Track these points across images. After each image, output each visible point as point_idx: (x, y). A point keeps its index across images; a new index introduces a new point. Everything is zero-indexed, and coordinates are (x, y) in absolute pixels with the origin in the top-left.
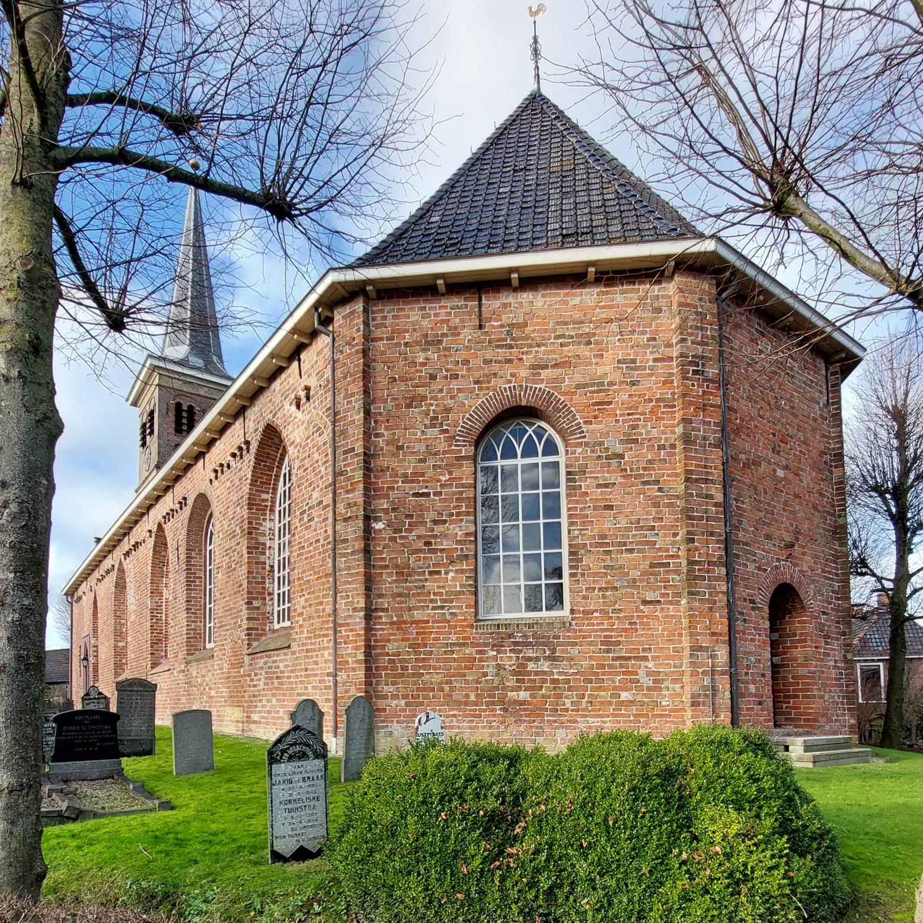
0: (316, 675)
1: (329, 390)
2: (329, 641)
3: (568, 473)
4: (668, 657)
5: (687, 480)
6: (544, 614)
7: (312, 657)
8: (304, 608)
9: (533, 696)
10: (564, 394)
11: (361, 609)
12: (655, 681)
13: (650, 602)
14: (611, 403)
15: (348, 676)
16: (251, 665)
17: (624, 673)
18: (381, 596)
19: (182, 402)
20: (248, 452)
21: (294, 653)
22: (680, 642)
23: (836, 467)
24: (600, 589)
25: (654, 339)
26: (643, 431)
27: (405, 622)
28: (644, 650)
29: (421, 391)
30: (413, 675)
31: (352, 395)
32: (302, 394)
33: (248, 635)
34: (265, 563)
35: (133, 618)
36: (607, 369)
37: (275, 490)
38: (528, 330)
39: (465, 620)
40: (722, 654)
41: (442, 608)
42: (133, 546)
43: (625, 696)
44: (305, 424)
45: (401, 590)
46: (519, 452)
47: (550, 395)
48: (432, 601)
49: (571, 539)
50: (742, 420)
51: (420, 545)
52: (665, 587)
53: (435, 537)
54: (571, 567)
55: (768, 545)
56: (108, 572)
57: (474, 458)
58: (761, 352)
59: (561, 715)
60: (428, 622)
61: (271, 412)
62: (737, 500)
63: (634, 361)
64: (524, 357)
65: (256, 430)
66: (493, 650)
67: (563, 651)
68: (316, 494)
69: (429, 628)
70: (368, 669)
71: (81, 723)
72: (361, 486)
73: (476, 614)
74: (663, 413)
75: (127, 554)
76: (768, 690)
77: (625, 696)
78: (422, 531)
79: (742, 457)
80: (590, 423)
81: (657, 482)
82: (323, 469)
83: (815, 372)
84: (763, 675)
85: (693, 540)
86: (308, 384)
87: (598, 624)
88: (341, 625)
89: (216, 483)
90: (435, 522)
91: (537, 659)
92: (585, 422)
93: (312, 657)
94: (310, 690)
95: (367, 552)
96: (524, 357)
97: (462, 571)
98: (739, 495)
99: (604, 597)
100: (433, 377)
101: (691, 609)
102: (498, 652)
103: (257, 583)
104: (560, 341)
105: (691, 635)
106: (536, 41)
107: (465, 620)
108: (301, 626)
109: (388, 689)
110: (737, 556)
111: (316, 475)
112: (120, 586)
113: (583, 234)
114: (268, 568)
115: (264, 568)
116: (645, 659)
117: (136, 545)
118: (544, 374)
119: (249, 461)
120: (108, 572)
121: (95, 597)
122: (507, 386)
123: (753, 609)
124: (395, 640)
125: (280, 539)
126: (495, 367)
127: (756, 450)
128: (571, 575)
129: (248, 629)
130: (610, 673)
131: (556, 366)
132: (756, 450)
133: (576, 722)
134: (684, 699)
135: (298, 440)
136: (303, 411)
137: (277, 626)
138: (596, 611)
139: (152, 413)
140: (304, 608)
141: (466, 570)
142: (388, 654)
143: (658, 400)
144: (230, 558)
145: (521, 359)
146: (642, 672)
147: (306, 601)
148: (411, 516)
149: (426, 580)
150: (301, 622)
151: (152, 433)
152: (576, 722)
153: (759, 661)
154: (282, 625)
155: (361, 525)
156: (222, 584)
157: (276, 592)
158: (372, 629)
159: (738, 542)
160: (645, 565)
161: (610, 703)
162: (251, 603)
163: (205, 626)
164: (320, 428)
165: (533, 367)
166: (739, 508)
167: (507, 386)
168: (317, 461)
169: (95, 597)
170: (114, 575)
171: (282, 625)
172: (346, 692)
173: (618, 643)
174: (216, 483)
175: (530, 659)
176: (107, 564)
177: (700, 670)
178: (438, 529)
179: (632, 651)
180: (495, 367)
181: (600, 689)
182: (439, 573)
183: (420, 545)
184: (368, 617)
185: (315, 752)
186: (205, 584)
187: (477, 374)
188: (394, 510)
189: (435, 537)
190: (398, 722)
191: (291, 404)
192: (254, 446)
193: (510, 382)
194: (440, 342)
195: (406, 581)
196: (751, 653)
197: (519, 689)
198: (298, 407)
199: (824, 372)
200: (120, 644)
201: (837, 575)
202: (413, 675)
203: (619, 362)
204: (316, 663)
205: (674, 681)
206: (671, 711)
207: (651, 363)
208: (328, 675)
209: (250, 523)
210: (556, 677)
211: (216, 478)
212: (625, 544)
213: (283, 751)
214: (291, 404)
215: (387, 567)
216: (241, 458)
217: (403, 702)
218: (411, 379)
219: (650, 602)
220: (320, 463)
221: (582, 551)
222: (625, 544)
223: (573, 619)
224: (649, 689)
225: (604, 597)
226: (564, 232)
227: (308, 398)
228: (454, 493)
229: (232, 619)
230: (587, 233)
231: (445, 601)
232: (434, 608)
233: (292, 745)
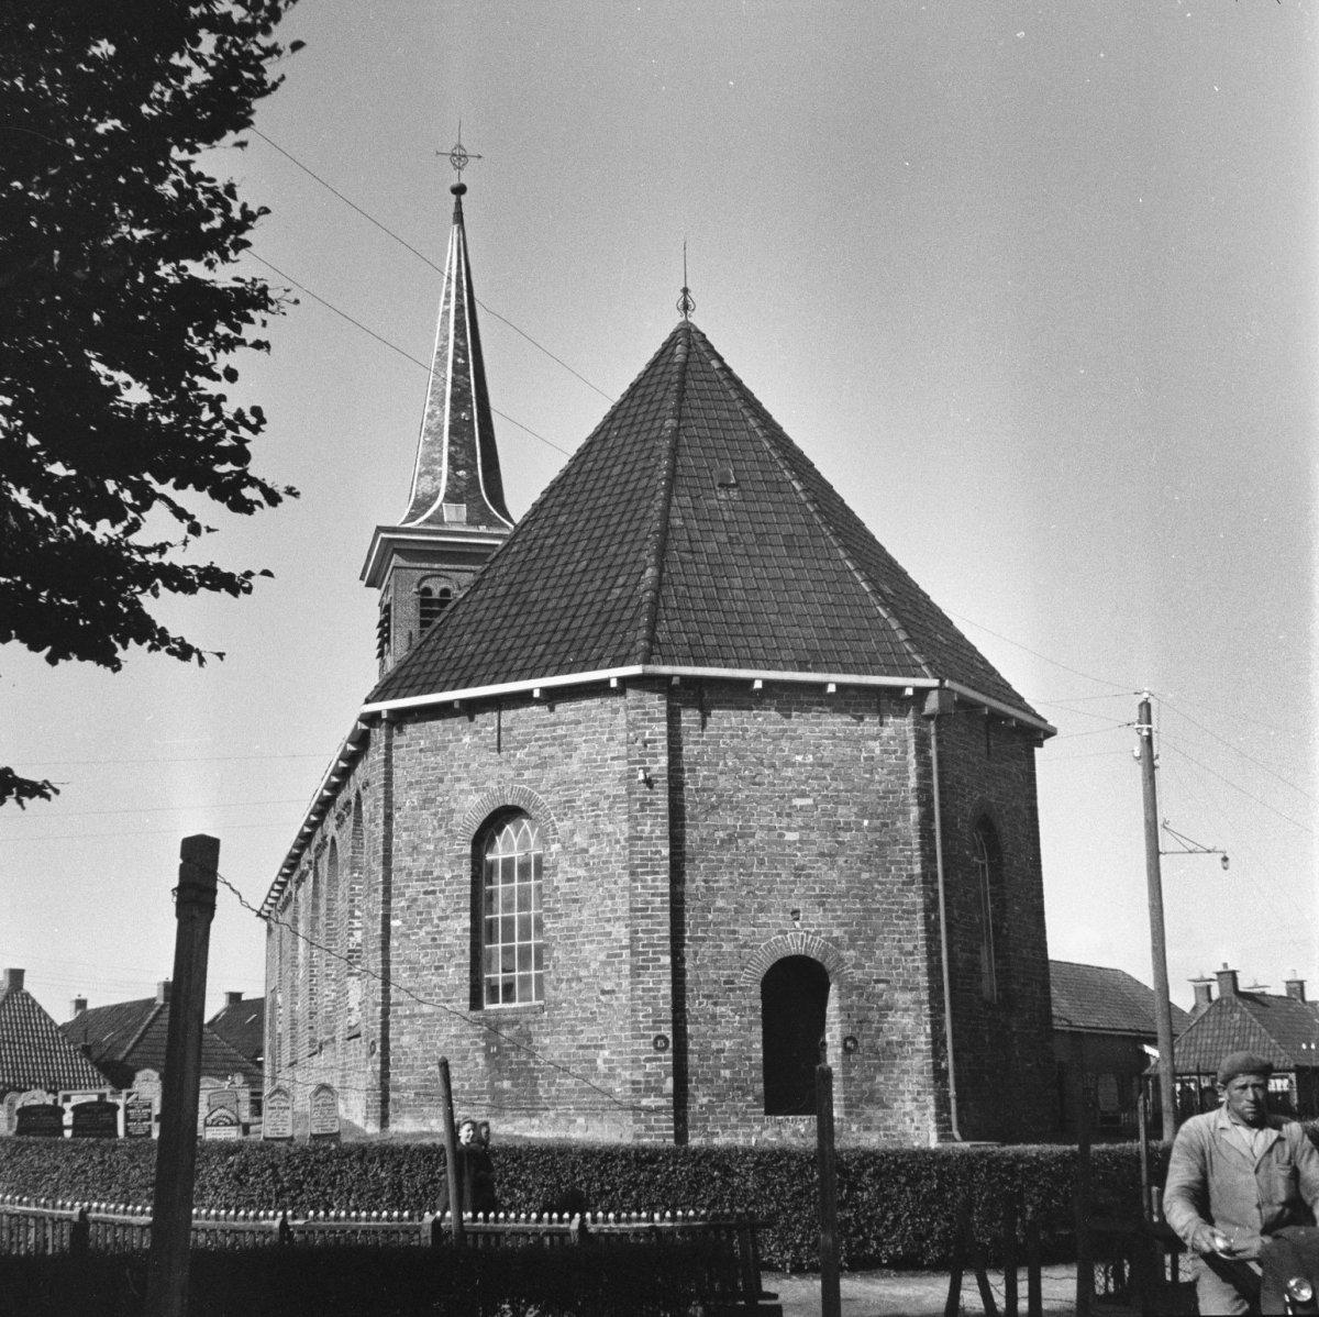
6: (500, 1005)
10: (541, 793)
13: (608, 992)
19: (431, 586)
38: (515, 733)
47: (531, 794)
53: (439, 933)
71: (88, 1112)
78: (428, 928)
90: (441, 919)
106: (685, 291)
146: (599, 1062)
160: (602, 957)
165: (516, 769)
178: (443, 925)
189: (439, 933)
194: (445, 748)
219: (608, 992)
229: (657, 887)
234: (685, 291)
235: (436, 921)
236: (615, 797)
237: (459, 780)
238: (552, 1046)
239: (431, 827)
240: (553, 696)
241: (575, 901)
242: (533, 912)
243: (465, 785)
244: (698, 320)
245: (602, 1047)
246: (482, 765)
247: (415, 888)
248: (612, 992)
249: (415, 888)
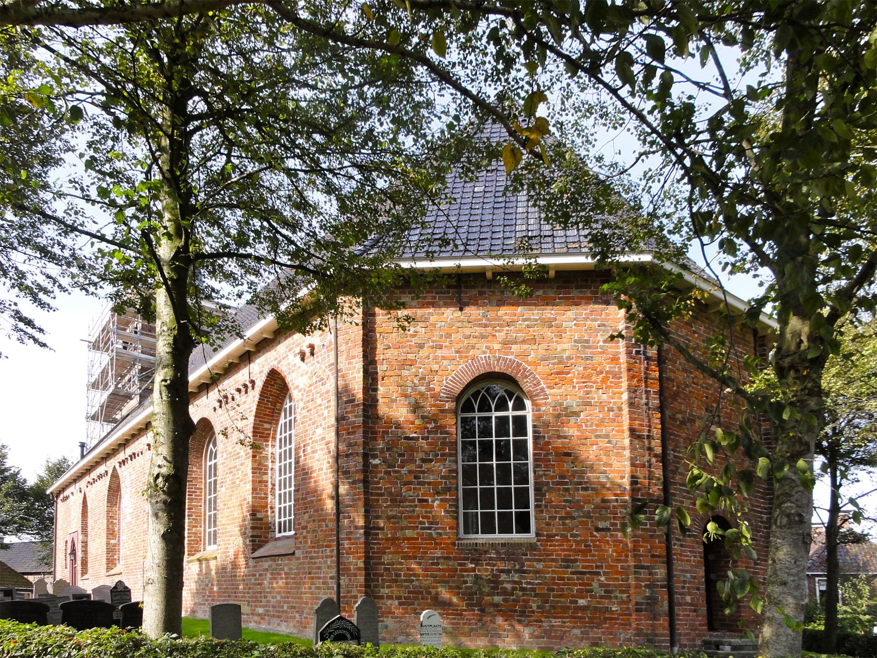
0: (319, 578)
1: (331, 350)
2: (332, 551)
4: (618, 573)
7: (315, 563)
8: (308, 522)
9: (505, 600)
10: (530, 364)
11: (362, 528)
12: (606, 592)
14: (569, 373)
15: (350, 580)
16: (256, 566)
17: (581, 585)
18: (378, 517)
20: (253, 388)
21: (298, 559)
22: (626, 561)
23: (764, 421)
24: (561, 518)
25: (604, 325)
26: (595, 396)
27: (398, 539)
28: (597, 567)
29: (410, 356)
30: (405, 581)
31: (353, 357)
32: (307, 351)
33: (253, 541)
34: (267, 482)
35: (128, 519)
36: (565, 348)
39: (449, 538)
40: (661, 572)
41: (429, 528)
42: (130, 456)
43: (582, 602)
44: (309, 374)
45: (394, 513)
46: (493, 407)
48: (421, 523)
49: (536, 478)
50: (678, 387)
52: (614, 518)
53: (423, 472)
54: (536, 500)
56: (100, 477)
57: (455, 412)
58: (695, 332)
59: (528, 616)
60: (417, 539)
61: (276, 359)
62: (674, 451)
63: (587, 341)
64: (497, 334)
65: (261, 372)
66: (471, 563)
67: (529, 566)
68: (319, 431)
69: (419, 544)
72: (361, 430)
73: (457, 534)
74: (611, 382)
75: (124, 462)
76: (702, 601)
77: (582, 602)
78: (412, 467)
79: (679, 416)
81: (607, 436)
82: (326, 412)
83: (745, 345)
84: (698, 589)
86: (312, 343)
87: (558, 546)
88: (343, 539)
89: (219, 411)
90: (424, 461)
91: (508, 572)
92: (548, 387)
93: (315, 563)
94: (313, 589)
95: (366, 482)
96: (497, 334)
97: (446, 500)
98: (676, 446)
99: (564, 524)
100: (421, 346)
101: (635, 536)
102: (476, 565)
103: (260, 498)
104: (527, 323)
105: (635, 556)
107: (449, 538)
108: (305, 537)
109: (385, 591)
110: (674, 495)
111: (320, 416)
112: (114, 491)
113: (545, 236)
114: (270, 486)
115: (267, 486)
116: (598, 574)
117: (133, 456)
118: (515, 348)
119: (254, 397)
120: (100, 477)
121: (85, 498)
122: (483, 356)
124: (390, 553)
125: (280, 462)
126: (473, 341)
127: (691, 411)
128: (536, 506)
129: (252, 536)
130: (568, 584)
131: (524, 342)
132: (691, 411)
133: (541, 621)
134: (630, 606)
135: (301, 386)
136: (307, 363)
137: (278, 535)
138: (557, 535)
140: (308, 522)
141: (449, 500)
142: (383, 564)
143: (607, 372)
144: (234, 475)
145: (494, 336)
146: (595, 585)
147: (310, 517)
148: (403, 455)
149: (416, 506)
150: (304, 534)
152: (541, 621)
153: (694, 578)
154: (283, 534)
155: (361, 460)
156: (225, 497)
157: (277, 506)
158: (370, 543)
159: (675, 484)
161: (569, 608)
162: (255, 515)
163: (205, 531)
164: (322, 379)
166: (675, 456)
167: (483, 356)
168: (320, 405)
169: (85, 498)
170: (106, 480)
171: (283, 534)
172: (349, 592)
173: (575, 561)
174: (219, 411)
175: (503, 571)
176: (101, 469)
177: (643, 584)
178: (425, 466)
179: (587, 567)
180: (473, 341)
181: (560, 596)
182: (427, 501)
183: (411, 478)
184: (367, 534)
185: (351, 634)
186: (205, 494)
187: (458, 346)
188: (388, 449)
189: (423, 472)
190: (392, 618)
191: (295, 356)
192: (259, 384)
193: (484, 353)
195: (399, 506)
196: (687, 571)
197: (493, 594)
198: (303, 359)
199: (752, 345)
200: (112, 542)
201: (765, 508)
202: (405, 581)
203: (575, 341)
204: (319, 568)
205: (622, 592)
206: (619, 615)
207: (601, 343)
208: (331, 578)
210: (524, 585)
211: (221, 407)
212: (581, 483)
213: (331, 633)
214: (295, 356)
215: (382, 495)
216: (246, 392)
217: (396, 603)
218: (403, 347)
219: (602, 530)
220: (323, 407)
221: (545, 488)
222: (581, 483)
223: (538, 541)
224: (601, 597)
225: (564, 524)
226: (530, 234)
227: (312, 354)
228: (438, 438)
230: (549, 236)
231: (432, 523)
232: (423, 529)
233: (336, 629)
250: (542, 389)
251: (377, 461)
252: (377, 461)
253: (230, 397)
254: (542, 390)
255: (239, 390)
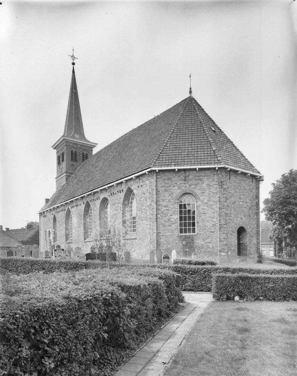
3: (197, 206)
5: (219, 209)
6: (188, 234)
11: (155, 233)
25: (214, 180)
37: (129, 201)
51: (167, 220)
55: (237, 219)
70: (157, 245)
78: (167, 217)
80: (201, 197)
81: (214, 209)
84: (235, 246)
85: (220, 220)
90: (170, 216)
106: (190, 89)
123: (233, 233)
128: (197, 226)
139: (63, 154)
147: (141, 229)
151: (63, 160)
164: (145, 193)
171: (131, 233)
178: (171, 217)
209: (123, 208)
216: (120, 193)
234: (190, 89)
235: (169, 216)
236: (214, 192)
237: (174, 186)
238: (199, 242)
239: (167, 196)
240: (201, 169)
241: (204, 213)
242: (191, 215)
243: (176, 188)
244: (194, 95)
245: (211, 243)
246: (180, 184)
247: (163, 209)
248: (213, 232)
249: (163, 209)
250: (199, 197)
251: (159, 216)
252: (159, 216)
253: (115, 193)
254: (199, 197)
255: (118, 192)
